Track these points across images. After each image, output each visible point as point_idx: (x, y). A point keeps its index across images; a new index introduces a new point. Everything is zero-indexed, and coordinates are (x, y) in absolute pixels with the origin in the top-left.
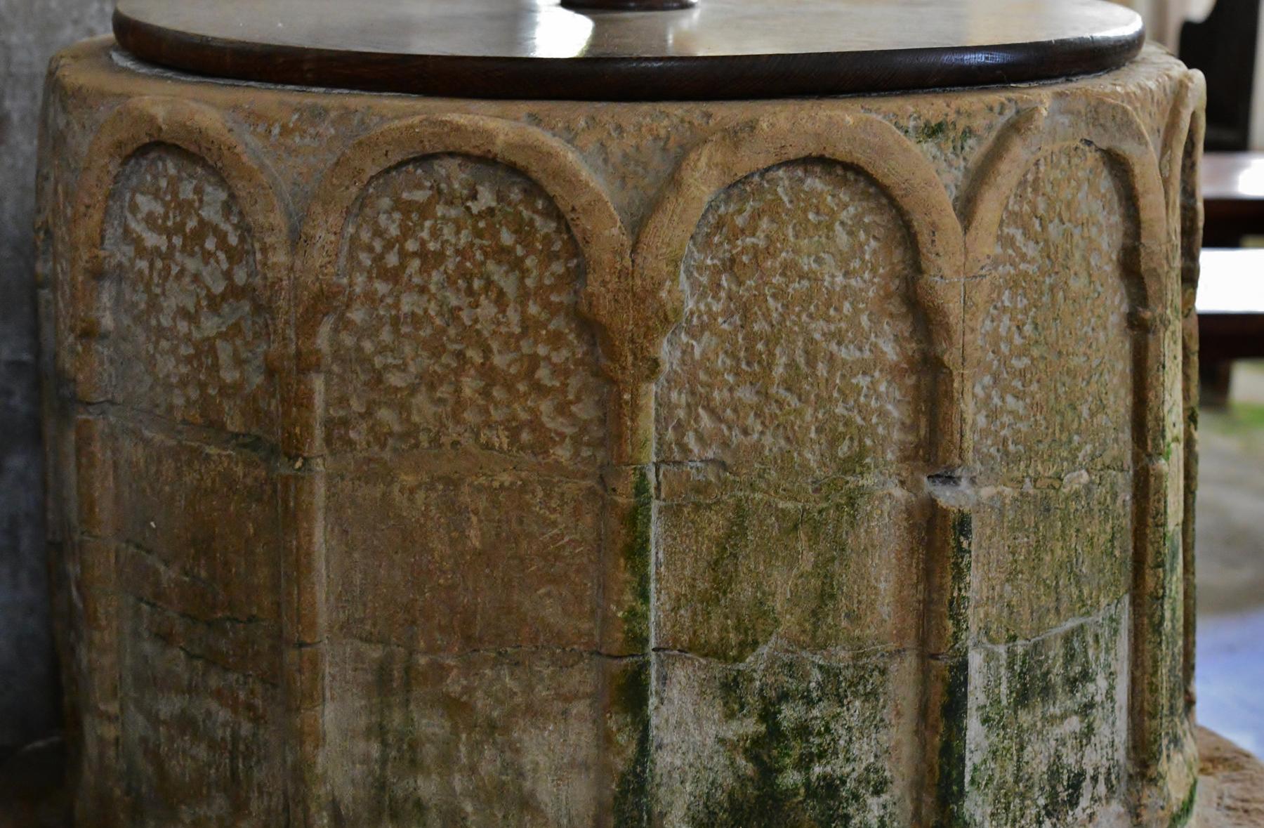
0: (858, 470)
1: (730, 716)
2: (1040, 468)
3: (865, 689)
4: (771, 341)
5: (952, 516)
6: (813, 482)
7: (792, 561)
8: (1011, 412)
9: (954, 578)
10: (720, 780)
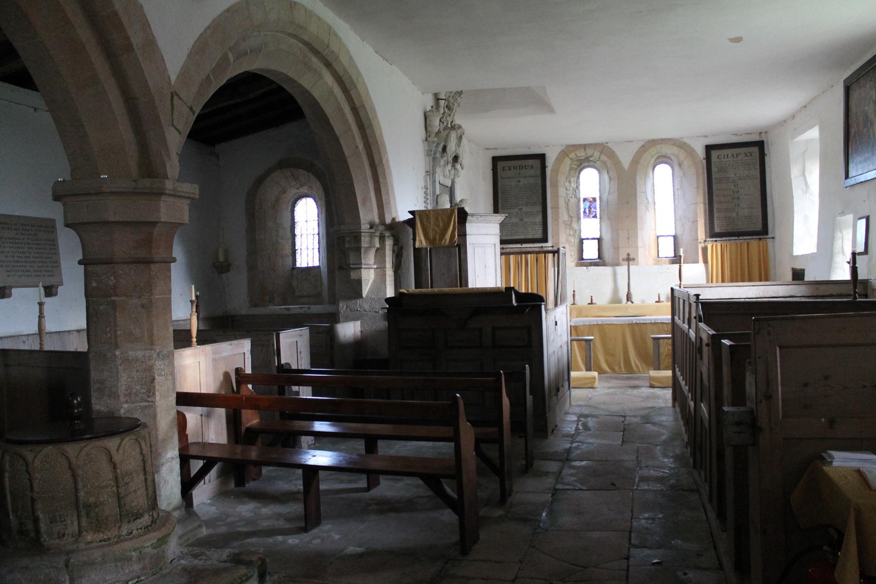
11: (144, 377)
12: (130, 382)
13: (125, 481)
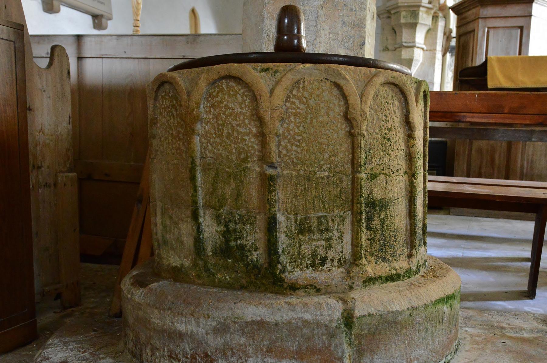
0: (246, 162)
1: (218, 225)
2: (306, 167)
3: (250, 221)
4: (223, 125)
5: (267, 176)
6: (235, 164)
7: (230, 185)
8: (295, 151)
9: (268, 193)
10: (217, 242)
11: (352, 35)
12: (333, 40)
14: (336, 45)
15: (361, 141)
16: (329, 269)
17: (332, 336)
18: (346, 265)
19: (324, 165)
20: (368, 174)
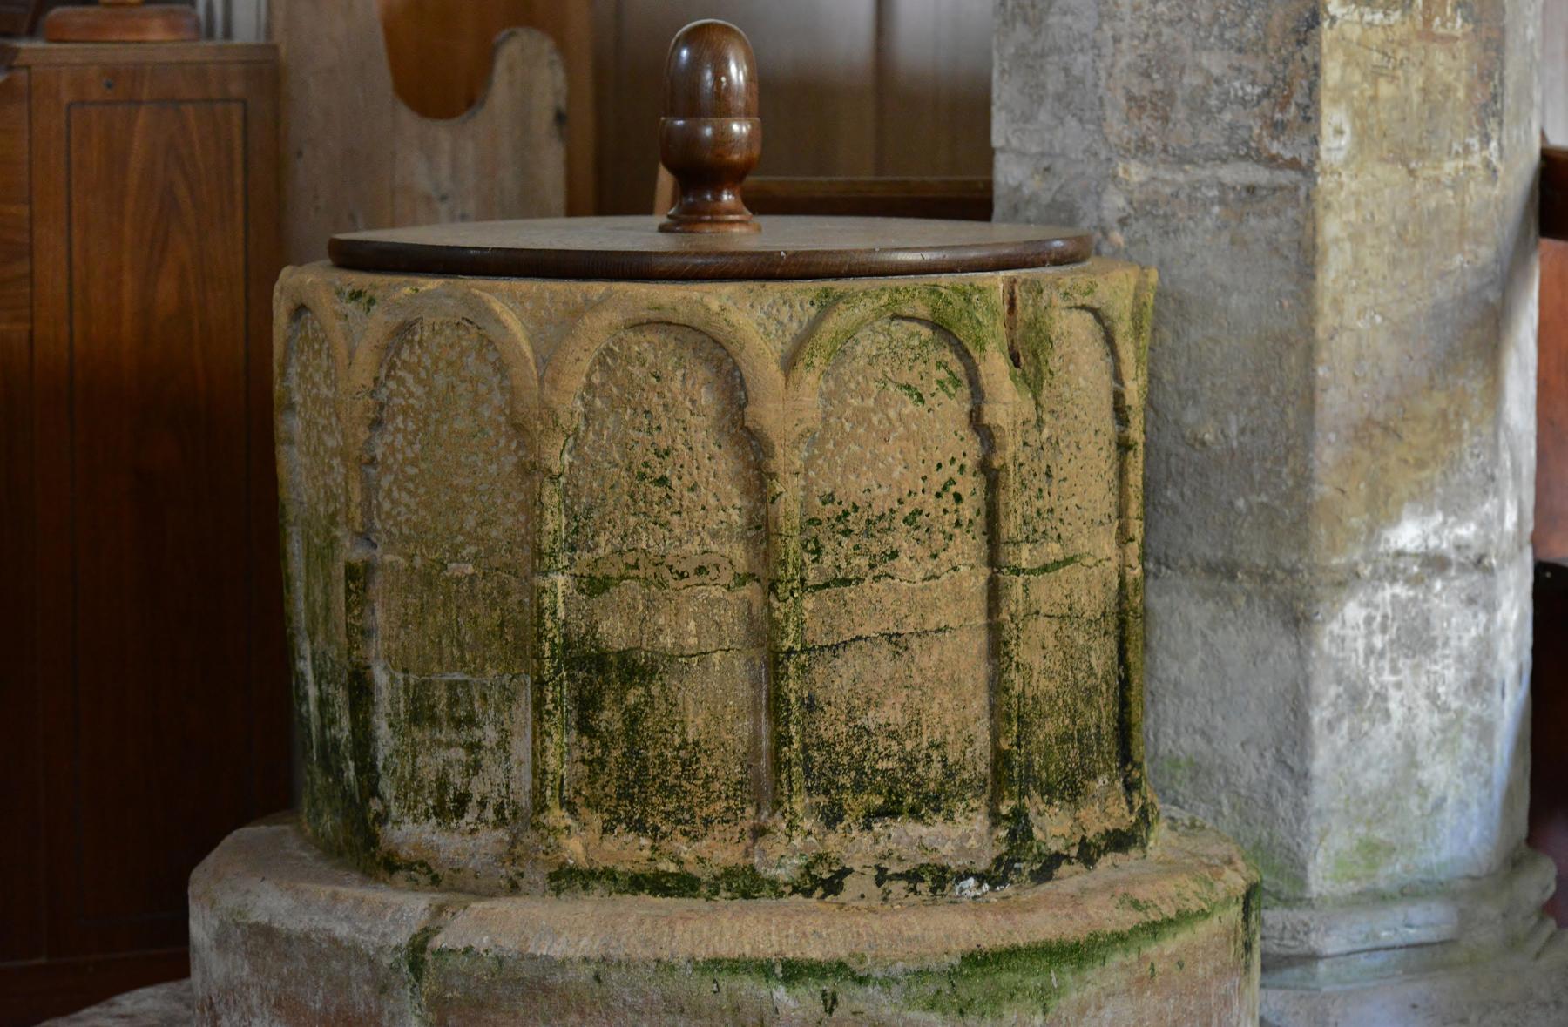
12: (1171, 23)
13: (827, 561)
14: (1185, 42)
15: (541, 487)
16: (472, 826)
17: (383, 989)
18: (516, 823)
19: (463, 545)
20: (582, 576)
